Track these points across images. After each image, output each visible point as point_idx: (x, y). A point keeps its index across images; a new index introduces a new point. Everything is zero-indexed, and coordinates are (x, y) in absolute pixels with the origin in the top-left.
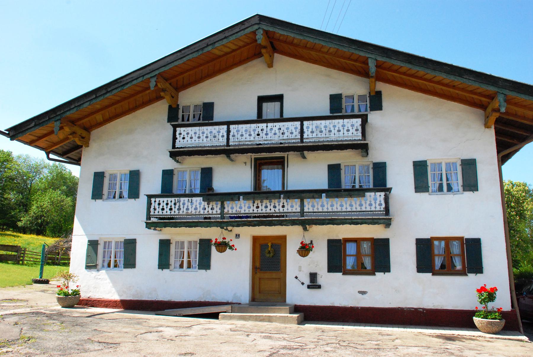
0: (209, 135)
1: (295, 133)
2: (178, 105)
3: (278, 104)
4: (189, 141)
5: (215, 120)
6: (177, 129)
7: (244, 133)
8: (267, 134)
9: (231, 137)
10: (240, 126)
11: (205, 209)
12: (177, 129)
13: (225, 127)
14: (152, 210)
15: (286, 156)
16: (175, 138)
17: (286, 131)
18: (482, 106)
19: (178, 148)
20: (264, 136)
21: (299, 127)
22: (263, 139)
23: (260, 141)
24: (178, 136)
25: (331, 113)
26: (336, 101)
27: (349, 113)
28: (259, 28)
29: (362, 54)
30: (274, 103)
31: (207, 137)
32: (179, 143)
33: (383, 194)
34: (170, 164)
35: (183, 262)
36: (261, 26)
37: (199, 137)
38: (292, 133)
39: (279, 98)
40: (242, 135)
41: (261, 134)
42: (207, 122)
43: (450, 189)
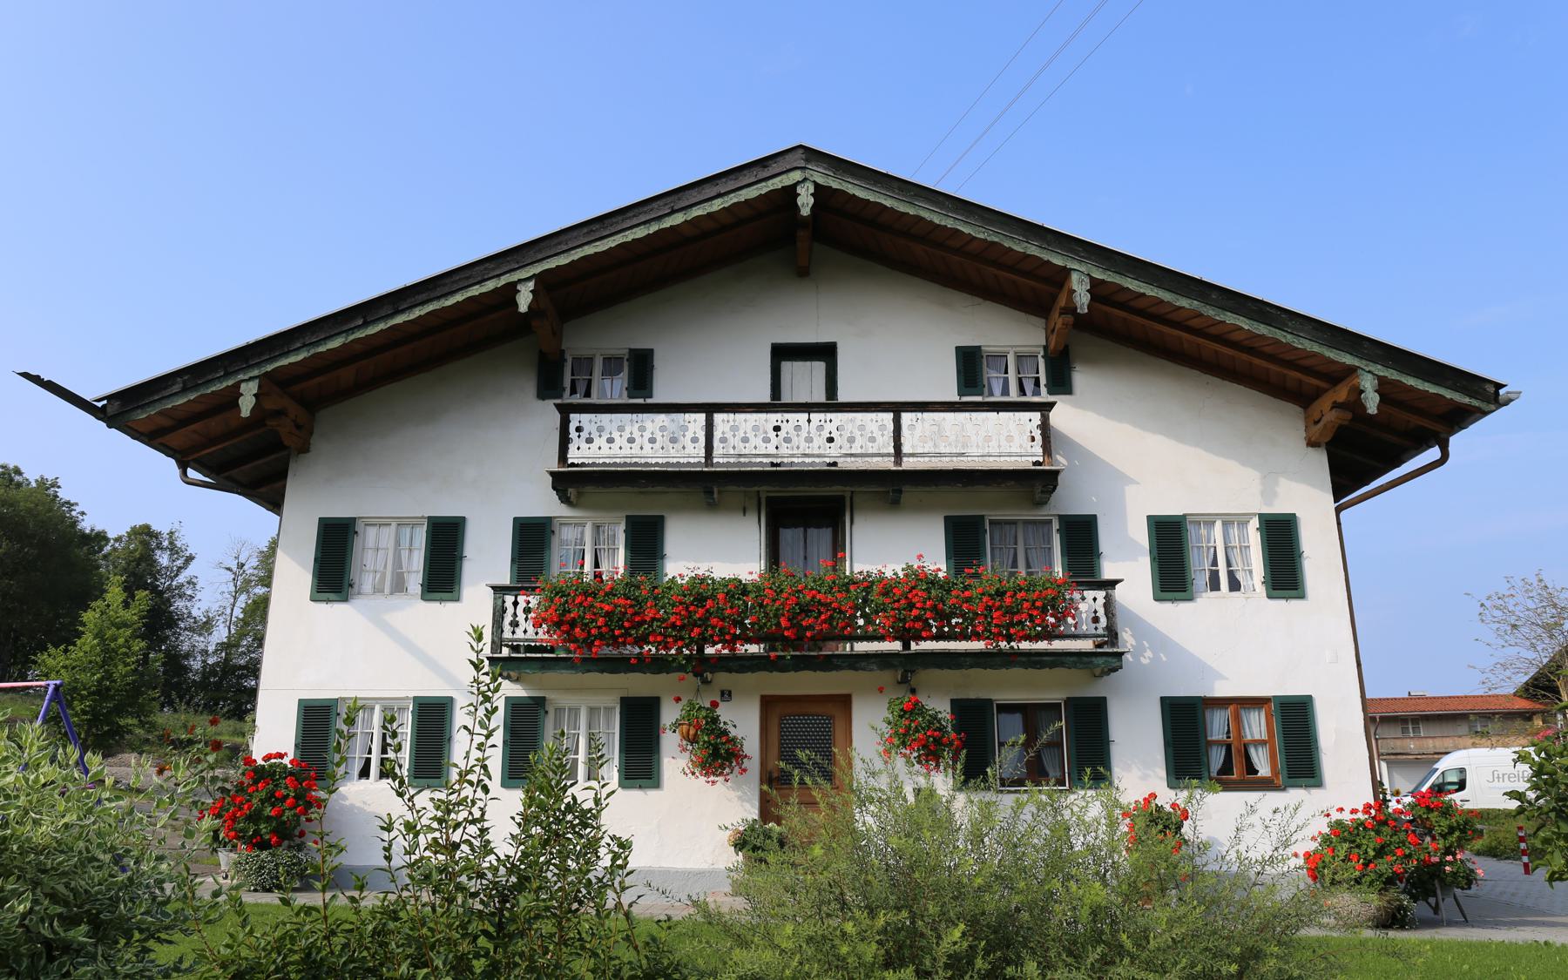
0: (658, 435)
1: (880, 440)
2: (562, 352)
3: (819, 367)
4: (605, 451)
5: (659, 397)
6: (572, 416)
7: (750, 435)
8: (809, 440)
9: (716, 443)
10: (740, 417)
11: (517, 625)
12: (572, 416)
13: (701, 417)
14: (507, 628)
15: (848, 496)
16: (564, 442)
17: (857, 434)
18: (1301, 398)
19: (573, 465)
20: (803, 445)
21: (891, 427)
22: (801, 451)
23: (793, 456)
24: (573, 434)
25: (960, 394)
26: (970, 365)
27: (998, 398)
28: (805, 179)
29: (1058, 261)
30: (808, 363)
31: (652, 441)
32: (580, 453)
33: (1101, 595)
34: (543, 503)
35: (368, 761)
36: (807, 174)
37: (631, 440)
38: (872, 440)
39: (826, 353)
40: (745, 440)
41: (795, 439)
42: (1410, 381)
43: (1235, 585)
